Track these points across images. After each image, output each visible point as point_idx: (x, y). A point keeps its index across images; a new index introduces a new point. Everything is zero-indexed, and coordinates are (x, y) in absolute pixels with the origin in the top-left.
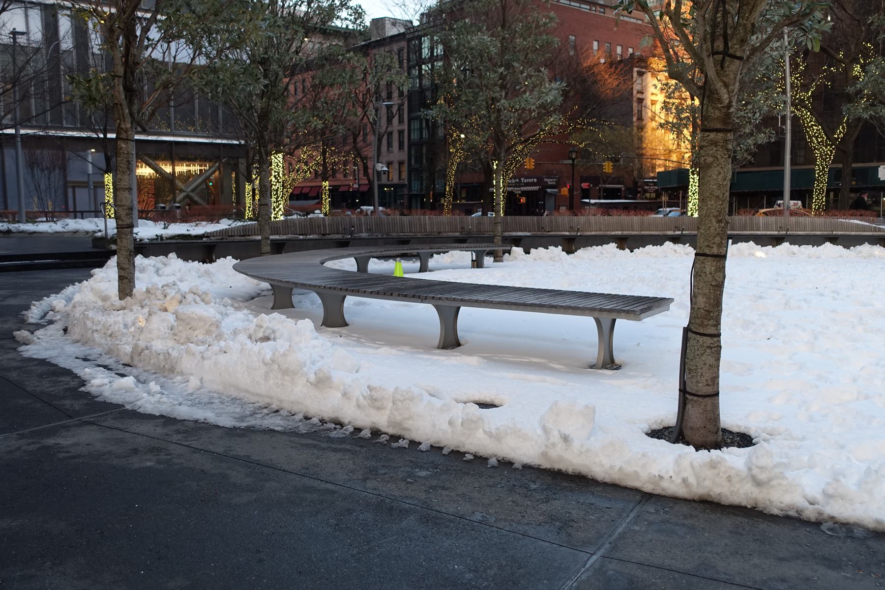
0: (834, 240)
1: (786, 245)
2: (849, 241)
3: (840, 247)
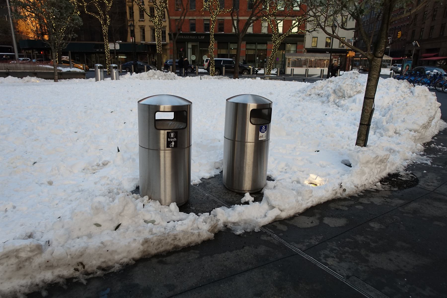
0: (14, 74)
1: (10, 77)
2: (21, 75)
3: (16, 78)
